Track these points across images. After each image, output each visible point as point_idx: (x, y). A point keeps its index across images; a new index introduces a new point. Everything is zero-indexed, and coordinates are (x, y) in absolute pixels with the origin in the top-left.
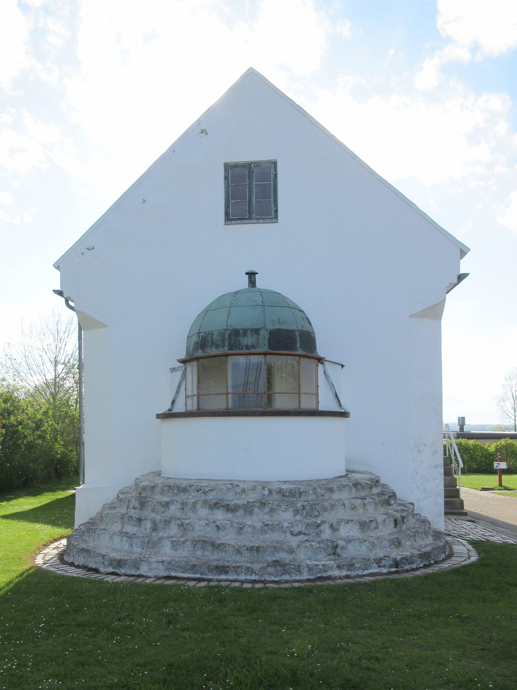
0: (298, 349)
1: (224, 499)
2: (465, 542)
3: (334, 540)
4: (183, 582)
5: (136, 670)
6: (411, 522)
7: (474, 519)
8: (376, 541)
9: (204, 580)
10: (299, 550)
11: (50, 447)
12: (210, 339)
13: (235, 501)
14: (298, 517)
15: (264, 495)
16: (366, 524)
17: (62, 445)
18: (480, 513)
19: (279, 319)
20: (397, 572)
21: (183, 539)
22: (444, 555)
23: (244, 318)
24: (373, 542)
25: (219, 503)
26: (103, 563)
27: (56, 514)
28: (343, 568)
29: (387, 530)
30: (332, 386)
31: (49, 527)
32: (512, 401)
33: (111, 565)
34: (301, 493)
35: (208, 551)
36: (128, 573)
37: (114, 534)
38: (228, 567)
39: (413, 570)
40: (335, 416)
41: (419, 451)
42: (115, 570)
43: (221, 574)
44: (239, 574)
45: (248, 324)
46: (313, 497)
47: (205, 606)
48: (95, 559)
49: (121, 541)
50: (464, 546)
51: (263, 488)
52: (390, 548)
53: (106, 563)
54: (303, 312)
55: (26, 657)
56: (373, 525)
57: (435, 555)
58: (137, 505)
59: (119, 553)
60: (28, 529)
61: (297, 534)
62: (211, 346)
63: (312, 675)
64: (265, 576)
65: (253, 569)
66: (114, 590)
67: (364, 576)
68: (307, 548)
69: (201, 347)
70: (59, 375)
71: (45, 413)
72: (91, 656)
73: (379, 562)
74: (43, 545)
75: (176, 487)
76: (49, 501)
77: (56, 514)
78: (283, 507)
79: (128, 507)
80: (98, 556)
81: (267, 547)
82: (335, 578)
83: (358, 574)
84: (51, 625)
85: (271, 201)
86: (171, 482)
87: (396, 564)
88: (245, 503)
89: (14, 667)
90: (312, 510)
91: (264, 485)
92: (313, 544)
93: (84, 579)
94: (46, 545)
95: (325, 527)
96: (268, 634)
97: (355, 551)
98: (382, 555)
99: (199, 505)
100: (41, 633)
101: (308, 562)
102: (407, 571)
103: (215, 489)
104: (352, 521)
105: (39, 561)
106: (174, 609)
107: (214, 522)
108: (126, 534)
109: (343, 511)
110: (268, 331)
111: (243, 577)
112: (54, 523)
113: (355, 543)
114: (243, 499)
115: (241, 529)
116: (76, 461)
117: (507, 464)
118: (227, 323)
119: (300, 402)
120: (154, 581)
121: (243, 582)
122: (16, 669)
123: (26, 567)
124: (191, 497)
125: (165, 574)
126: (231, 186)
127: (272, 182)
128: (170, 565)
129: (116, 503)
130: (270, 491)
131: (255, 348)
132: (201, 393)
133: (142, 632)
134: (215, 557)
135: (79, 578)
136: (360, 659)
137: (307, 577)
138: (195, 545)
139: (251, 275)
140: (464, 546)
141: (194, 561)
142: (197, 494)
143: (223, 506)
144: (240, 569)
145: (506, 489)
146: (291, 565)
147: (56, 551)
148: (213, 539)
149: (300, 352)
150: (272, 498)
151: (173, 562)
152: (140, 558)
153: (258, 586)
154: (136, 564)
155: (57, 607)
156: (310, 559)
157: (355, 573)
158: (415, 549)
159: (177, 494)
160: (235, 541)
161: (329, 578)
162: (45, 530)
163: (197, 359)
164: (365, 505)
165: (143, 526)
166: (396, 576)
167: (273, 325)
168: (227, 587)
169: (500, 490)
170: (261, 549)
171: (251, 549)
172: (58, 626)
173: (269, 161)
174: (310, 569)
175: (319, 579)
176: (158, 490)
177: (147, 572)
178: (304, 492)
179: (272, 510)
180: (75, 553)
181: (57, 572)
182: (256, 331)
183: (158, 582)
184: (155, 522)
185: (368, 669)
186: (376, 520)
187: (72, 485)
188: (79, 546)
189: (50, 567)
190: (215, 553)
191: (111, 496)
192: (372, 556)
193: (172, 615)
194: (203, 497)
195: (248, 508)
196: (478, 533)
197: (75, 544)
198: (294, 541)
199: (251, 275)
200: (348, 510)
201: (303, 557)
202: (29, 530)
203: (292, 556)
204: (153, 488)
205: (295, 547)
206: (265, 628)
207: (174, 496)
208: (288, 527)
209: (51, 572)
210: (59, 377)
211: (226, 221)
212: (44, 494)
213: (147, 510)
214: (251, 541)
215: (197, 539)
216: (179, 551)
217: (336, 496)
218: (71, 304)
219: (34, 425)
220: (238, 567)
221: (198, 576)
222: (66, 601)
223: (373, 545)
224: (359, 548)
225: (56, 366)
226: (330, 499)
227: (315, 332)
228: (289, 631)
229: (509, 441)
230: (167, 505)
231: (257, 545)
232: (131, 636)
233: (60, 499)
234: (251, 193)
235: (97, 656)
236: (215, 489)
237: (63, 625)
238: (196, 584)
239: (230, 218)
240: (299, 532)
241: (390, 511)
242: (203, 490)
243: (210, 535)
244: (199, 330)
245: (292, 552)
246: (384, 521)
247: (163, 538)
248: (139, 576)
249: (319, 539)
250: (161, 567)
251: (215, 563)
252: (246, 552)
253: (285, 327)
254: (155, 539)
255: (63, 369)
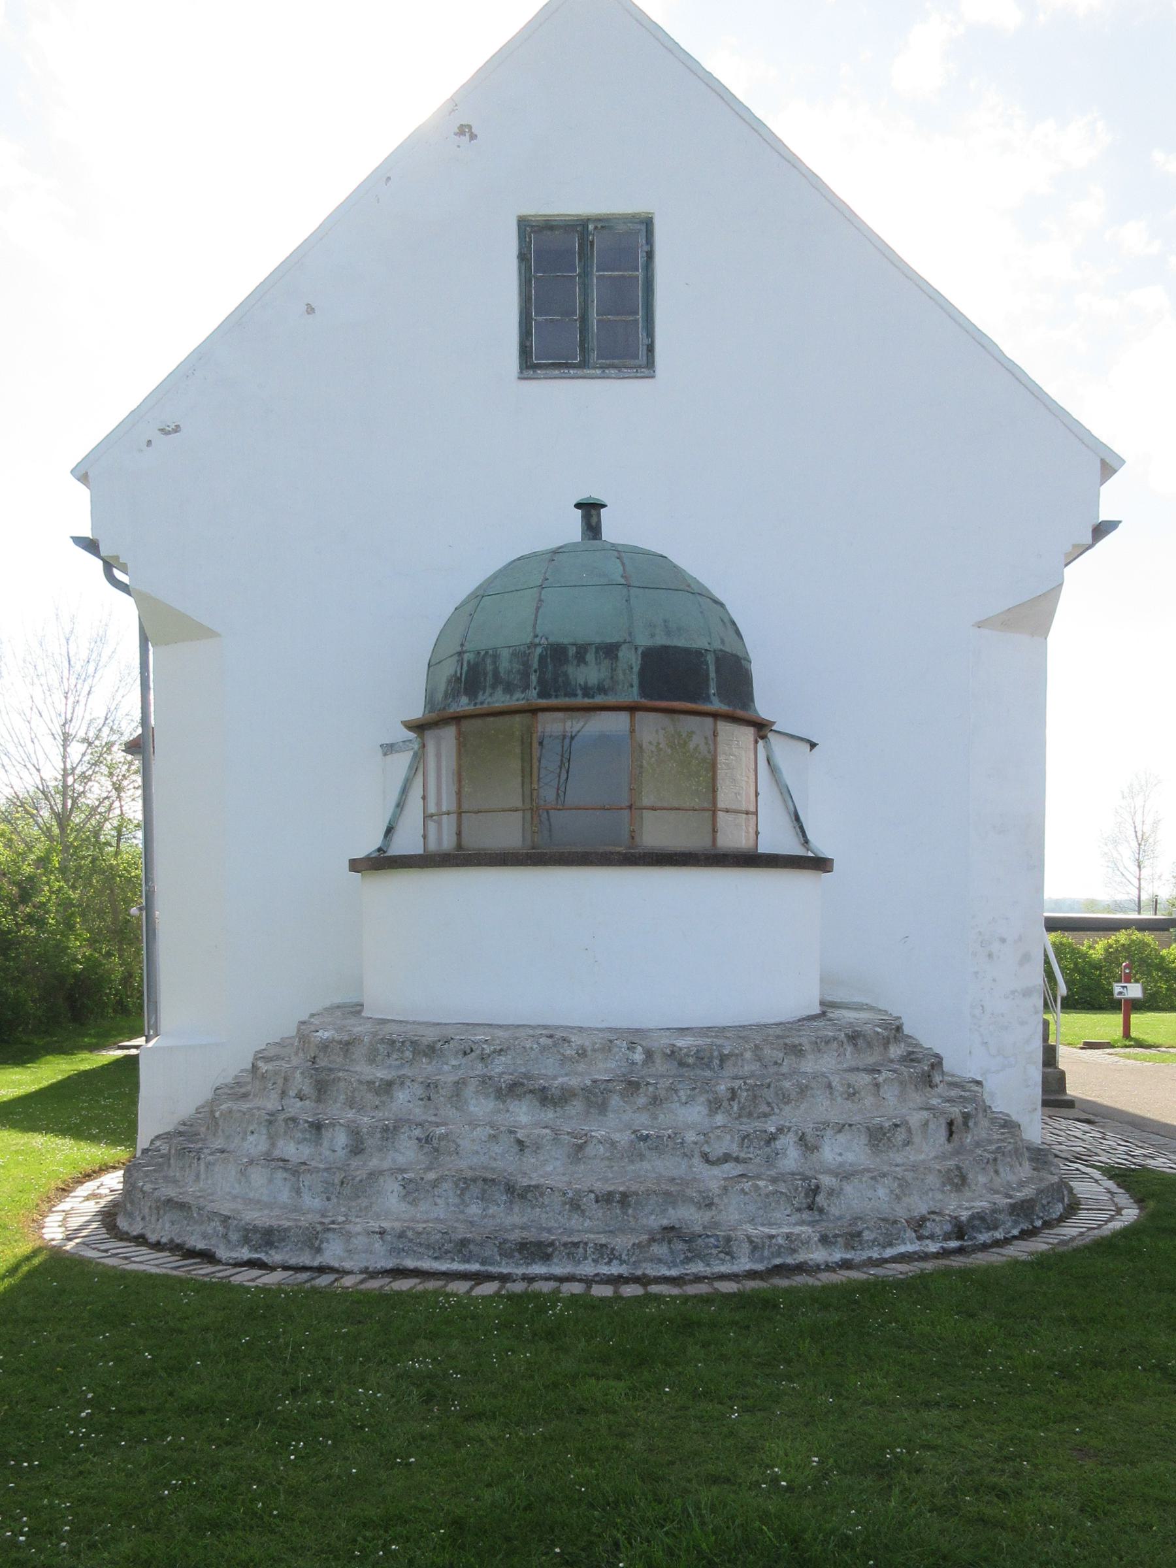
0: (713, 698)
1: (530, 1071)
2: (1096, 1174)
3: (809, 1173)
4: (431, 1285)
5: (365, 1538)
6: (981, 1129)
7: (1091, 1117)
8: (909, 1175)
9: (490, 1277)
10: (726, 1201)
11: (57, 946)
12: (489, 668)
13: (560, 1080)
14: (720, 1119)
15: (634, 1063)
16: (884, 1134)
17: (88, 940)
18: (1099, 1100)
19: (665, 621)
20: (960, 1251)
21: (431, 1176)
22: (1061, 1205)
23: (579, 618)
24: (903, 1178)
25: (522, 1084)
26: (225, 1236)
27: (82, 1108)
28: (834, 1243)
29: (930, 1148)
30: (785, 793)
31: (68, 1142)
32: (1135, 844)
33: (246, 1240)
34: (723, 1059)
35: (499, 1205)
36: (293, 1262)
37: (251, 1162)
38: (552, 1244)
39: (997, 1243)
40: (804, 868)
41: (990, 956)
42: (256, 1256)
43: (533, 1262)
44: (579, 1262)
45: (588, 632)
46: (753, 1068)
47: (513, 1352)
48: (203, 1228)
49: (270, 1181)
50: (1096, 1181)
51: (632, 1046)
52: (943, 1192)
53: (234, 1237)
54: (722, 605)
55: (51, 1506)
56: (901, 1135)
57: (1044, 1206)
58: (307, 1089)
59: (266, 1212)
60: (13, 1148)
61: (718, 1159)
62: (494, 687)
63: (846, 1543)
64: (644, 1265)
65: (613, 1249)
66: (265, 1309)
67: (886, 1261)
68: (746, 1194)
69: (465, 689)
70: (73, 769)
71: (43, 861)
72: (234, 1502)
73: (920, 1226)
74: (58, 1189)
75: (408, 1044)
76: (60, 1077)
77: (82, 1108)
78: (682, 1093)
79: (284, 1093)
80: (210, 1220)
81: (649, 1193)
82: (816, 1269)
83: (870, 1258)
84: (110, 1411)
85: (636, 321)
86: (393, 1031)
87: (960, 1230)
88: (588, 1083)
89: (22, 1538)
90: (750, 1101)
91: (634, 1037)
92: (761, 1183)
93: (180, 1280)
94: (65, 1191)
95: (788, 1142)
96: (694, 1425)
97: (861, 1200)
98: (922, 1209)
99: (469, 1091)
100: (87, 1436)
101: (751, 1230)
102: (985, 1247)
103: (508, 1048)
104: (850, 1125)
105: (53, 1231)
106: (435, 1359)
107: (511, 1132)
108: (281, 1164)
109: (827, 1103)
110: (640, 651)
111: (588, 1269)
112: (77, 1132)
113: (861, 1181)
114: (581, 1074)
115: (580, 1147)
116: (122, 979)
117: (1145, 990)
118: (534, 627)
119: (715, 831)
120: (362, 1282)
121: (588, 1281)
122: (29, 1545)
123: (24, 1248)
124: (448, 1070)
125: (390, 1265)
126: (537, 279)
127: (640, 274)
128: (402, 1239)
129: (247, 1083)
130: (649, 1054)
131: (606, 694)
132: (465, 807)
133: (362, 1427)
134: (515, 1221)
135: (167, 1276)
136: (953, 1491)
137: (747, 1267)
138: (463, 1190)
139: (590, 510)
140: (1096, 1181)
141: (462, 1232)
142: (464, 1061)
143: (531, 1091)
144: (581, 1250)
145: (1140, 1044)
146: (708, 1236)
147: (92, 1207)
148: (510, 1174)
149: (717, 705)
150: (653, 1070)
151: (410, 1234)
152: (322, 1223)
153: (629, 1290)
154: (313, 1239)
155: (119, 1360)
156: (752, 1221)
157: (865, 1255)
158: (997, 1192)
159: (411, 1063)
160: (566, 1179)
161: (800, 1268)
162: (60, 1152)
163: (457, 719)
164: (877, 1085)
165: (326, 1143)
166: (957, 1262)
167: (653, 636)
168: (555, 1295)
169: (1126, 1047)
170: (633, 1200)
171: (606, 1199)
172: (130, 1413)
173: (634, 216)
174: (755, 1247)
175: (779, 1270)
176: (359, 1052)
177: (342, 1260)
178: (731, 1055)
179: (655, 1101)
180: (147, 1210)
181: (103, 1260)
182: (610, 651)
183: (374, 1284)
184: (358, 1133)
185: (983, 1520)
186: (907, 1123)
187: (115, 1036)
188: (156, 1194)
189: (83, 1247)
190: (516, 1209)
191: (233, 1062)
192: (901, 1213)
193: (431, 1376)
194: (480, 1069)
195: (595, 1095)
196: (1116, 1150)
197: (148, 1188)
198: (712, 1178)
199: (590, 510)
200: (839, 1099)
201: (733, 1214)
202: (16, 1152)
203: (707, 1216)
204: (347, 1046)
205: (717, 1191)
206: (684, 1408)
207: (402, 1066)
208: (696, 1143)
209: (90, 1260)
210: (73, 773)
211: (521, 372)
212: (43, 1059)
213: (335, 1101)
214: (606, 1180)
215: (469, 1174)
216: (423, 1206)
217: (809, 1065)
218: (118, 574)
219: (15, 890)
220: (576, 1245)
221: (475, 1267)
222: (142, 1342)
223: (904, 1184)
224: (870, 1193)
225: (65, 746)
226: (795, 1072)
227: (752, 656)
228: (747, 1417)
229: (1137, 935)
230: (387, 1087)
231: (621, 1189)
232: (334, 1440)
233: (85, 1073)
234: (585, 296)
235: (253, 1501)
236: (508, 1048)
237: (142, 1411)
238: (472, 1288)
239: (534, 359)
240: (725, 1154)
241: (934, 1102)
242: (478, 1052)
243: (500, 1164)
244: (462, 645)
245: (710, 1205)
246: (926, 1124)
247: (381, 1173)
248: (322, 1270)
249: (772, 1173)
250: (378, 1245)
251: (516, 1236)
252: (595, 1206)
253: (681, 643)
254: (361, 1174)
255: (84, 755)
